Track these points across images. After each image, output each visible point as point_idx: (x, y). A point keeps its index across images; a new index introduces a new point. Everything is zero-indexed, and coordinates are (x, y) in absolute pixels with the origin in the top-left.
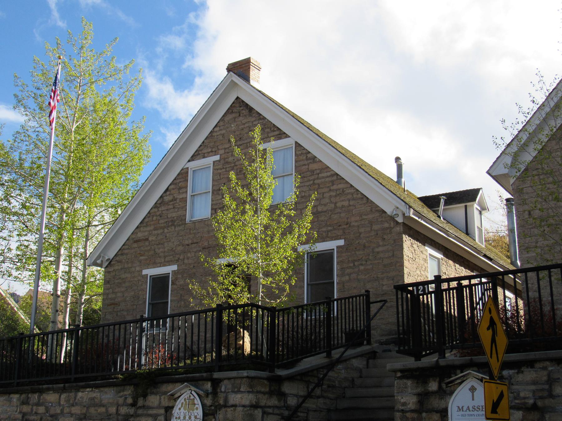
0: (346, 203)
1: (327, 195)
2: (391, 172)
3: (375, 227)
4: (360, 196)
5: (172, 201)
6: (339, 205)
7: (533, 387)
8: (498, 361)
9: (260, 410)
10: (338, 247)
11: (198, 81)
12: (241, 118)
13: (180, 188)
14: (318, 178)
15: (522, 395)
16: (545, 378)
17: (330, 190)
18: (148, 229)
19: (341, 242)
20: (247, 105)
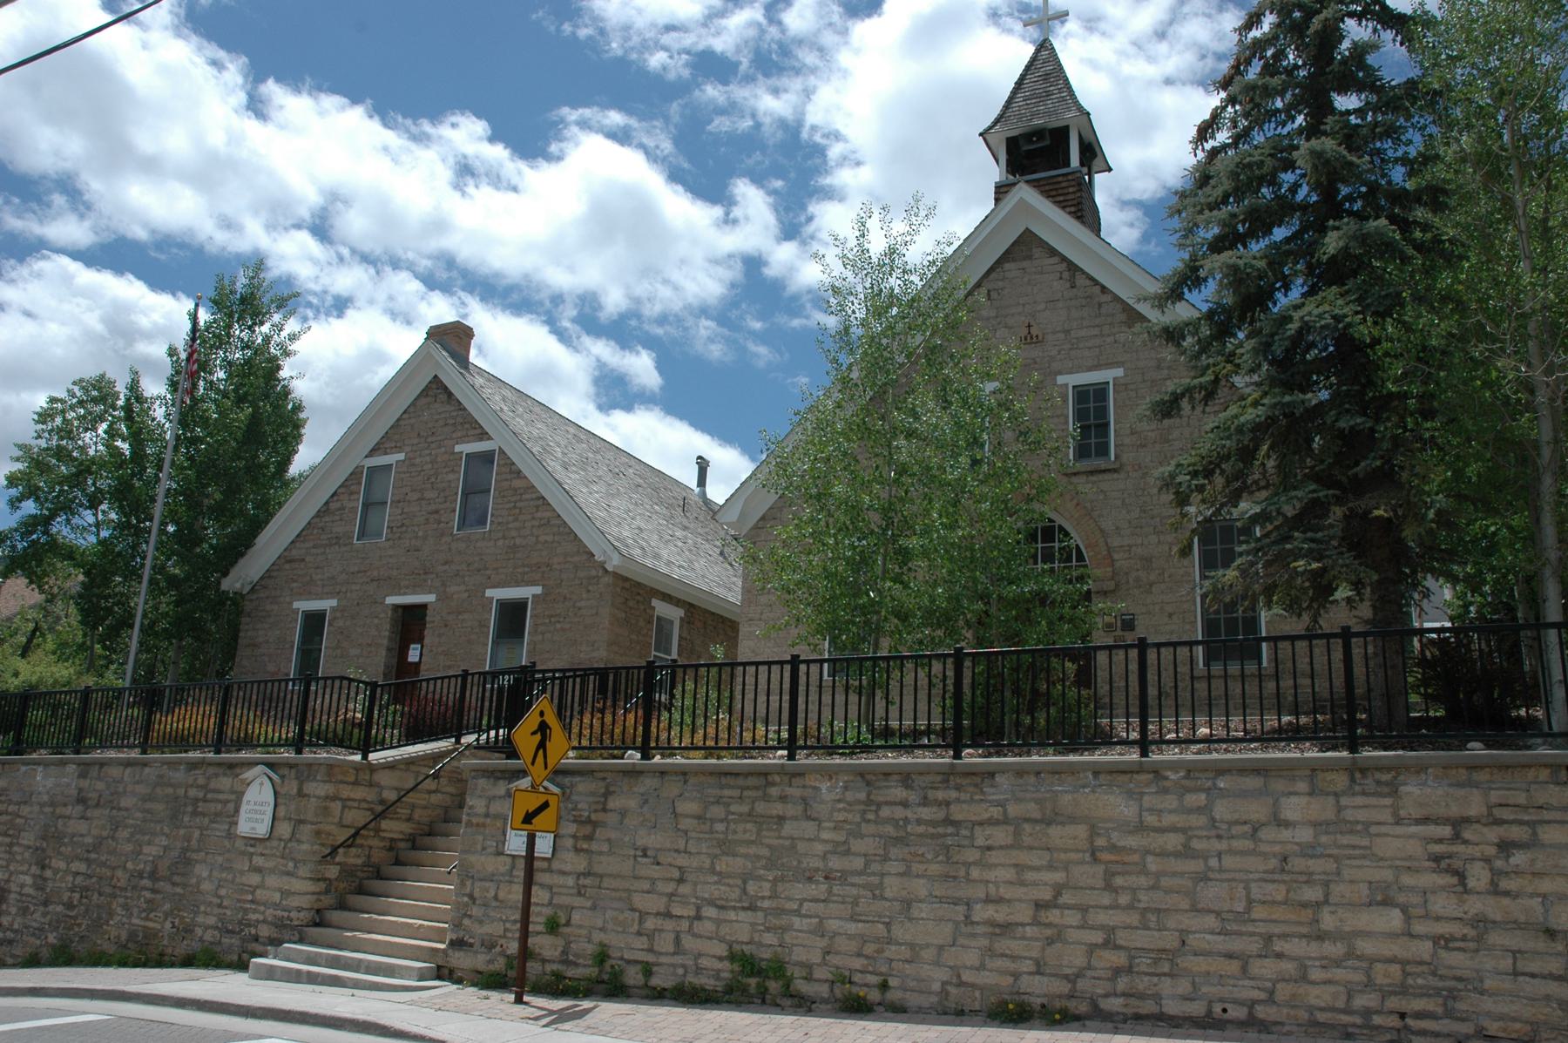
0: (550, 538)
1: (528, 524)
2: (690, 478)
3: (581, 574)
4: (567, 530)
5: (339, 509)
6: (542, 539)
7: (591, 799)
8: (546, 768)
9: (339, 804)
10: (533, 596)
11: (835, 151)
12: (436, 405)
13: (352, 493)
14: (521, 500)
15: (579, 806)
16: (603, 790)
17: (533, 518)
18: (307, 545)
19: (538, 590)
20: (446, 388)
